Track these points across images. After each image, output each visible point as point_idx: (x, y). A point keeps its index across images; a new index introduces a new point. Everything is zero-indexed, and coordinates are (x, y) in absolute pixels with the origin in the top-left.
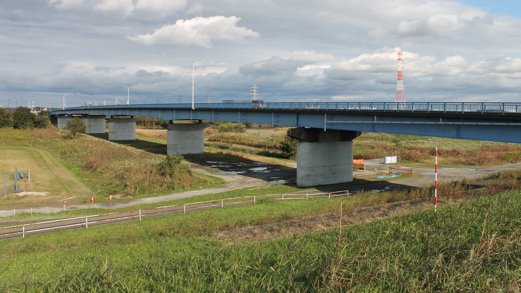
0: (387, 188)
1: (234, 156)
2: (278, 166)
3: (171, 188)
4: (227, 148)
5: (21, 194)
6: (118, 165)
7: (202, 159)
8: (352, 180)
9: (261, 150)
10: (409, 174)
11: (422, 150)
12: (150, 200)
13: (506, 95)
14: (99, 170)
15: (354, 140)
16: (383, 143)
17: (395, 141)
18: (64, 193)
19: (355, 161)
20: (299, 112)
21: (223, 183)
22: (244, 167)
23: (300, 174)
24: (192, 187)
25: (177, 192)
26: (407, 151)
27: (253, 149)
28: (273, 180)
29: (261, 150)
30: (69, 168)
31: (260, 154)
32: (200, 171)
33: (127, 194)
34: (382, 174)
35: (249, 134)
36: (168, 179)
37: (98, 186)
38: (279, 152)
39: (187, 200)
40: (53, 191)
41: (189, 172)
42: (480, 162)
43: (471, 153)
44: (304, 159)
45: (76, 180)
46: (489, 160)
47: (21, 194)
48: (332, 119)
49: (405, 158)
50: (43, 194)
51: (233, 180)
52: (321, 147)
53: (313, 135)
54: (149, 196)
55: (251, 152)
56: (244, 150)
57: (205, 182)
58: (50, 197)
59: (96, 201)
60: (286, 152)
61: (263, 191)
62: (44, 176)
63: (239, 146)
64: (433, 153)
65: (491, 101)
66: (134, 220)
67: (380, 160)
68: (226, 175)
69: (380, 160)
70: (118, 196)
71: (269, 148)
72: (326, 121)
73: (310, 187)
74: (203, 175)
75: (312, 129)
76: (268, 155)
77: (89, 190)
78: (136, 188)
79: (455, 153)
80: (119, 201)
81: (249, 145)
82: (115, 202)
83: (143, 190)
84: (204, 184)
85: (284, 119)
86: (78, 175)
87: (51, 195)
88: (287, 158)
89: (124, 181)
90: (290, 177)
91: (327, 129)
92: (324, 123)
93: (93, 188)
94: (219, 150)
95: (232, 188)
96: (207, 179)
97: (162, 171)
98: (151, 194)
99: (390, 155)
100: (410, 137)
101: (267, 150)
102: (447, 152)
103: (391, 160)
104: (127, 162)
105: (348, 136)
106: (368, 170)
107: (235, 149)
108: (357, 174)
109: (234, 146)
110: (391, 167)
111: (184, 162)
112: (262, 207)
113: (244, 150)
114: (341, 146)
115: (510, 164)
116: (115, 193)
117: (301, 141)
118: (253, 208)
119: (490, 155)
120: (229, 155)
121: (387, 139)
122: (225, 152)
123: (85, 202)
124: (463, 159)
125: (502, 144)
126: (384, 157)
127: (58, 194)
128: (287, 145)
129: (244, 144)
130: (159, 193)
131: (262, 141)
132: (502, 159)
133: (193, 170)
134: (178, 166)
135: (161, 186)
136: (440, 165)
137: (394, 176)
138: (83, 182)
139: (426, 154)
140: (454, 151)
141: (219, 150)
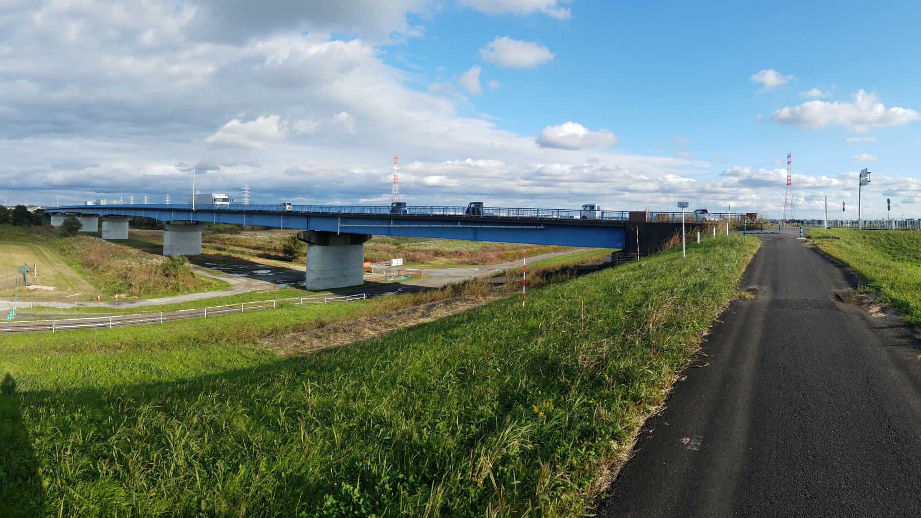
0: (400, 290)
1: (234, 258)
2: (282, 269)
3: (176, 290)
4: (225, 250)
5: (31, 287)
6: (121, 264)
7: (202, 261)
8: (627, 216)
9: (259, 252)
10: (417, 275)
11: (426, 252)
12: (156, 301)
13: (540, 201)
14: (101, 268)
15: (365, 244)
16: (386, 245)
17: (397, 245)
18: (70, 289)
19: (366, 265)
20: (309, 216)
21: (228, 287)
22: (249, 270)
23: (310, 277)
24: (197, 289)
25: (183, 294)
26: (412, 254)
27: (252, 251)
28: (279, 283)
29: (261, 252)
30: (70, 265)
31: (260, 256)
32: (202, 273)
33: (133, 294)
34: (390, 276)
35: (244, 236)
36: (173, 281)
37: (101, 284)
38: (281, 255)
39: (209, 302)
40: (59, 287)
41: (192, 273)
42: (483, 262)
43: (472, 254)
44: (311, 262)
45: (79, 277)
46: (492, 260)
47: (31, 287)
48: (345, 222)
49: (410, 260)
50: (51, 288)
51: (239, 283)
52: (331, 250)
53: (323, 239)
54: (154, 297)
55: (250, 254)
56: (242, 252)
57: (210, 284)
58: (57, 293)
59: (101, 300)
60: (289, 254)
61: (272, 295)
62: (48, 271)
63: (237, 248)
64: (437, 254)
65: (528, 207)
66: (157, 323)
67: (387, 264)
68: (230, 277)
69: (387, 264)
70: (123, 296)
71: (269, 250)
72: (302, 231)
73: (320, 291)
74: (205, 277)
75: (322, 232)
76: (269, 257)
77: (93, 288)
78: (141, 288)
79: (458, 254)
80: (125, 301)
81: (247, 247)
82: (120, 301)
83: (148, 291)
84: (209, 286)
85: (292, 222)
86: (80, 272)
87: (59, 289)
88: (290, 260)
89: (128, 280)
90: (296, 280)
91: (339, 231)
92: (338, 227)
93: (96, 286)
94: (216, 252)
95: (239, 291)
96: (211, 281)
97: (166, 272)
98: (156, 295)
99: (395, 258)
100: (410, 239)
101: (268, 252)
102: (443, 256)
103: (397, 262)
104: (126, 261)
105: (359, 239)
106: (375, 273)
107: (233, 251)
108: (367, 277)
109: (232, 248)
110: (399, 269)
111: (187, 264)
112: (283, 311)
113: (242, 252)
114: (352, 249)
115: (509, 263)
116: (120, 292)
117: (310, 244)
118: (273, 313)
119: (492, 255)
120: (229, 257)
121: (388, 242)
122: (224, 253)
123: (91, 300)
124: (467, 260)
125: (498, 244)
126: (390, 260)
127: (65, 290)
128: (290, 247)
129: (240, 246)
130: (164, 295)
131: (260, 243)
132: (502, 258)
133: (195, 272)
134: (181, 267)
135: (166, 287)
136: (445, 266)
137: (403, 278)
138: (86, 279)
139: (431, 256)
140: (457, 252)
141: (216, 252)
